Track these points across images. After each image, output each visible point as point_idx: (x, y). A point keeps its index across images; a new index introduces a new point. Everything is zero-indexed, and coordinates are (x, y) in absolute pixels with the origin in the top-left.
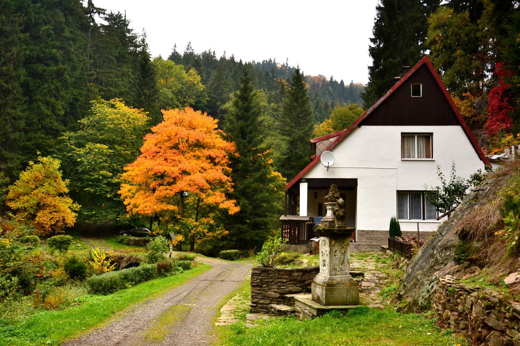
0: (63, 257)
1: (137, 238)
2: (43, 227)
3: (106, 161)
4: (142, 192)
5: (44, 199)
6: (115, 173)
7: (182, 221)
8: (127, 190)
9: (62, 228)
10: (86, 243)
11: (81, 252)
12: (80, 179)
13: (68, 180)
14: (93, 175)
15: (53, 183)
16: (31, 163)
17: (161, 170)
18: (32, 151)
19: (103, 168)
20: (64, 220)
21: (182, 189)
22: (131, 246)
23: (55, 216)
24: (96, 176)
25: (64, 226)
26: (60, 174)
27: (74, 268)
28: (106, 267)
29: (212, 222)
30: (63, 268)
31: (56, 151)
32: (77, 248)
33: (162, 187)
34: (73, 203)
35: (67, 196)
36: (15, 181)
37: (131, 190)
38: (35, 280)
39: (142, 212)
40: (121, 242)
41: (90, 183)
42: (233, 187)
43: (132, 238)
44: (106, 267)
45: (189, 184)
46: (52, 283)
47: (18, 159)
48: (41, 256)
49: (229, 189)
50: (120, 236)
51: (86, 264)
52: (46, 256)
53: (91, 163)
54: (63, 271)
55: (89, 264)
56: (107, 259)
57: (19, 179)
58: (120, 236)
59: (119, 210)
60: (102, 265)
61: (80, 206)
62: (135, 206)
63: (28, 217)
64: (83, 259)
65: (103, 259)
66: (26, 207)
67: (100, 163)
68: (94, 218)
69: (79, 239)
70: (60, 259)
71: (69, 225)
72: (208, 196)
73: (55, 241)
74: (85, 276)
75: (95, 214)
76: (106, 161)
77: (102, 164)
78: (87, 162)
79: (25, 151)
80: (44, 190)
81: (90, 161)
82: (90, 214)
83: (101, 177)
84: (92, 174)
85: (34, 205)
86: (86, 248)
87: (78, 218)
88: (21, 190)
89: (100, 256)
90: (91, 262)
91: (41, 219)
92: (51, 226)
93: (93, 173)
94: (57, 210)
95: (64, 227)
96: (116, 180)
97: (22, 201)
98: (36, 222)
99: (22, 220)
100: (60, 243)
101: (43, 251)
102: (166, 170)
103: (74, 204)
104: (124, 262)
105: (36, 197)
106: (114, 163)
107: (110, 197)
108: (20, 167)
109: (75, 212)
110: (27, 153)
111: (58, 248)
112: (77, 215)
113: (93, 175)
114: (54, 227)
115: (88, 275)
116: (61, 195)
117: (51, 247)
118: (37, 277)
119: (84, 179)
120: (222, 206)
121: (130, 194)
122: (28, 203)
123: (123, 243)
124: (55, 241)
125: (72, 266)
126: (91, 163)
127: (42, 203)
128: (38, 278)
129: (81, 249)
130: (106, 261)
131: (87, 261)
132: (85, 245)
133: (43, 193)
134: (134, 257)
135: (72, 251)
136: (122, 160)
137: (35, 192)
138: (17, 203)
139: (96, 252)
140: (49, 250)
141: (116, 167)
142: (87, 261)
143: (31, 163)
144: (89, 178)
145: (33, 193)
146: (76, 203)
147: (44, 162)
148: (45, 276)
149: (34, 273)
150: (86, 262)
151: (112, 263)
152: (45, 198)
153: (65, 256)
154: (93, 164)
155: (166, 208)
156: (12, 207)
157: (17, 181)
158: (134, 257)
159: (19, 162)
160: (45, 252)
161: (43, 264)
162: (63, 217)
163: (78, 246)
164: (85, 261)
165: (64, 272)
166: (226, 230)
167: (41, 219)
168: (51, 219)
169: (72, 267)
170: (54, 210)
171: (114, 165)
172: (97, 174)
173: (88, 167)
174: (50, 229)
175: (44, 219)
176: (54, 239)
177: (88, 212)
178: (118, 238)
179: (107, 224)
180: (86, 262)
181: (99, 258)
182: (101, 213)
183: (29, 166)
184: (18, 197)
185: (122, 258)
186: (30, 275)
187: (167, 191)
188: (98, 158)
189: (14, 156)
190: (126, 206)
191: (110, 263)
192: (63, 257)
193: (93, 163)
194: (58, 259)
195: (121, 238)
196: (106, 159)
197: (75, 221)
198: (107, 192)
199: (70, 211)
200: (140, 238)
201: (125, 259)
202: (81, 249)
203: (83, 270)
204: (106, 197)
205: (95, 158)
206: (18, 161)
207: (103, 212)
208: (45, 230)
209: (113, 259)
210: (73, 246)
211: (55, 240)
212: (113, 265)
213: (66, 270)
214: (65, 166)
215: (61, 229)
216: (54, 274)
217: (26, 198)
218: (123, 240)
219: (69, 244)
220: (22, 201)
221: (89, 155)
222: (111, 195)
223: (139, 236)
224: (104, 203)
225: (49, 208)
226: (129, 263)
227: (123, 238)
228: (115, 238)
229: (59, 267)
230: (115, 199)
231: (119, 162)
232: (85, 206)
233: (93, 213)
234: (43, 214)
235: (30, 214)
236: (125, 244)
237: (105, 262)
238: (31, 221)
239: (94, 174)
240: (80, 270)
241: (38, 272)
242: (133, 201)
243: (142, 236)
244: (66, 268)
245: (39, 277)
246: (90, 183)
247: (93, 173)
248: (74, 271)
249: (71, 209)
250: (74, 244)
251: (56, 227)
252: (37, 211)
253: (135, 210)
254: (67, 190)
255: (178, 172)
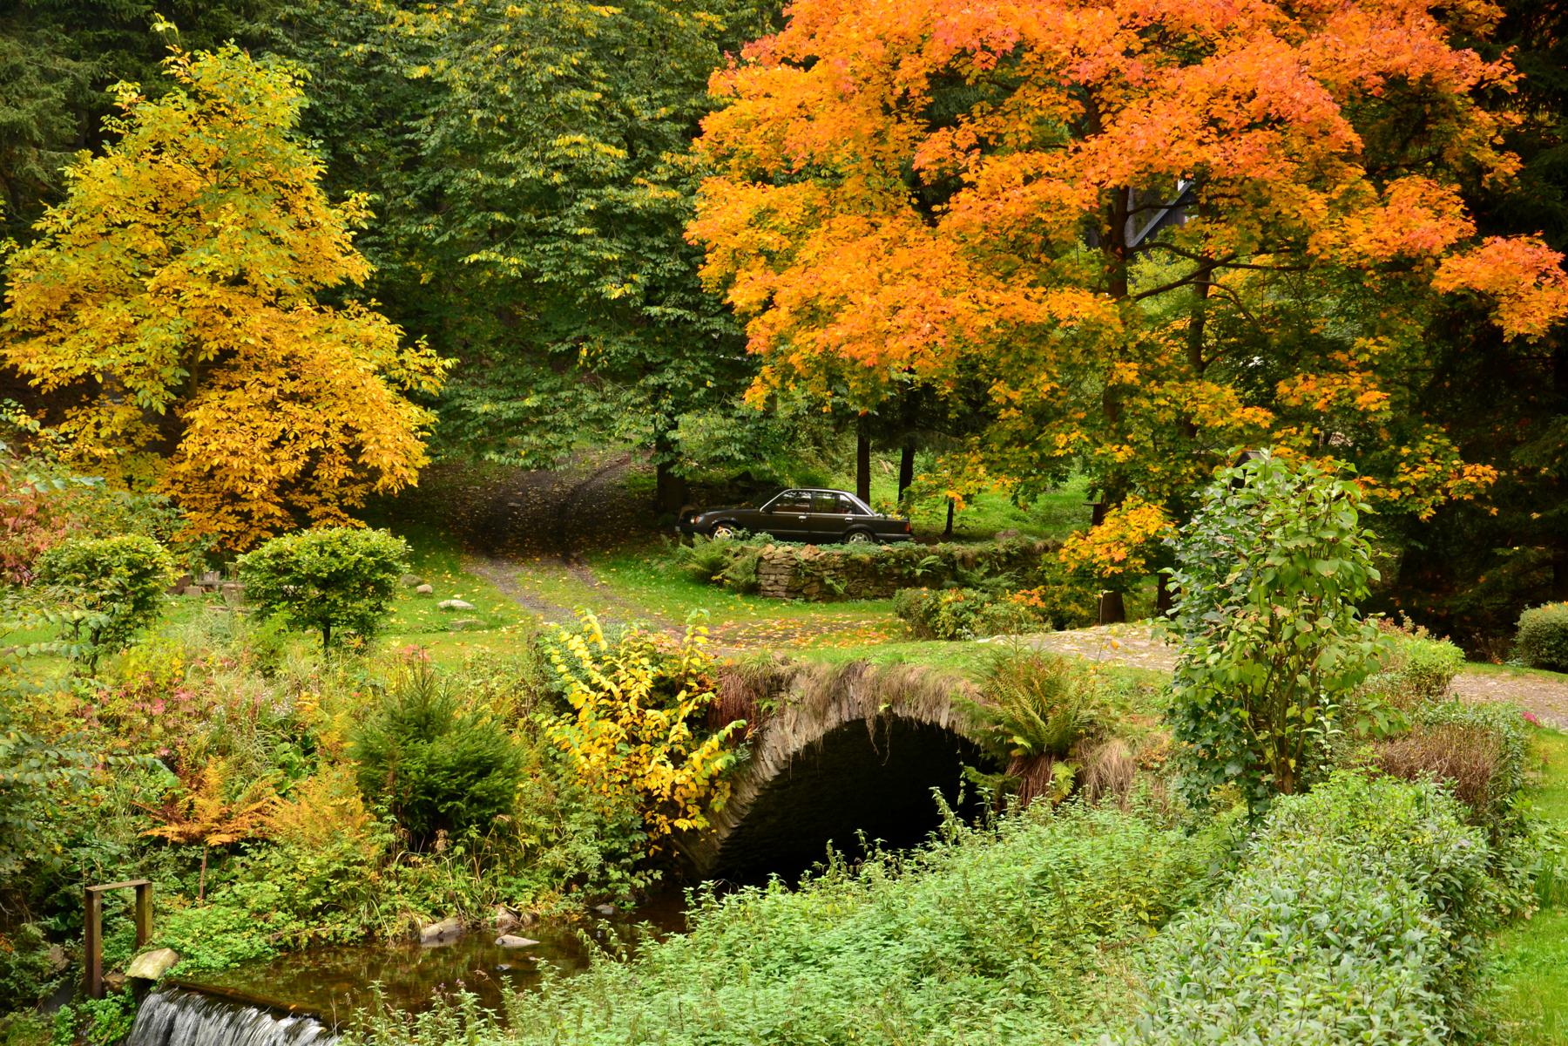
0: (346, 683)
1: (804, 552)
2: (234, 497)
3: (580, 77)
4: (845, 223)
5: (220, 318)
6: (643, 151)
7: (1146, 404)
8: (746, 212)
9: (348, 502)
10: (496, 590)
11: (474, 648)
12: (433, 202)
13: (364, 198)
14: (509, 169)
15: (269, 216)
16: (125, 93)
17: (997, 31)
18: (135, 35)
19: (571, 118)
20: (355, 451)
21: (1161, 163)
22: (774, 598)
23: (298, 427)
24: (532, 172)
25: (359, 490)
26: (308, 164)
27: (431, 769)
28: (660, 753)
29: (1373, 400)
30: (347, 772)
31: (279, 32)
32: (446, 623)
33: (997, 168)
34: (403, 345)
35: (362, 302)
36: (38, 213)
37: (771, 212)
38: (143, 871)
39: (867, 352)
40: (708, 577)
41: (499, 216)
42: (1512, 142)
43: (778, 550)
44: (660, 753)
45: (1214, 122)
46: (268, 891)
47: (48, 76)
48: (193, 682)
49: (1488, 155)
50: (697, 538)
51: (517, 738)
52: (221, 681)
53: (490, 89)
54: (347, 793)
55: (533, 730)
56: (664, 692)
57: (64, 199)
58: (697, 538)
59: (679, 382)
60: (634, 740)
61: (448, 363)
62: (811, 315)
63: (139, 441)
64: (489, 695)
65: (634, 696)
66: (119, 371)
67: (548, 88)
68: (532, 438)
69: (454, 570)
70: (325, 706)
71: (384, 479)
72: (1347, 210)
73: (288, 571)
74: (512, 827)
75: (538, 411)
76: (580, 77)
77: (559, 98)
78: (473, 87)
79: (90, 35)
80: (214, 263)
81: (486, 79)
82: (508, 411)
83: (558, 178)
84: (506, 158)
85: (163, 361)
86: (503, 622)
87: (437, 440)
88: (78, 268)
89: (613, 669)
90: (543, 718)
91: (213, 446)
92: (283, 487)
93: (512, 152)
94: (311, 388)
95: (363, 498)
96: (654, 192)
97: (92, 334)
98: (184, 468)
99: (100, 452)
100: (325, 584)
101: (202, 642)
102: (1034, 31)
103: (408, 354)
104: (790, 715)
105: (172, 311)
106: (632, 91)
107: (624, 300)
108: (68, 125)
109: (426, 401)
110: (105, 45)
111: (311, 621)
112: (431, 416)
113: (509, 169)
114: (300, 499)
115: (531, 820)
116: (330, 298)
117: (261, 616)
118: (161, 842)
119: (457, 194)
120: (1454, 275)
121: (770, 239)
122: (126, 347)
123: (720, 584)
124: (288, 571)
125: (413, 755)
126: (490, 89)
127: (214, 346)
128: (165, 853)
129: (470, 627)
130: (659, 706)
131: (519, 713)
132: (494, 600)
133: (213, 277)
134: (869, 673)
135: (412, 642)
136: (679, 73)
137: (163, 275)
138: (61, 349)
139: (578, 647)
140: (248, 633)
141: (647, 115)
142: (519, 713)
143: (125, 93)
144: (488, 187)
145: (151, 283)
146: (422, 342)
147: (206, 84)
148: (214, 840)
149: (137, 812)
150: (511, 723)
151: (701, 724)
152: (228, 314)
153: (359, 676)
154: (504, 100)
155: (1036, 314)
156: (31, 376)
157: (50, 211)
158: (869, 673)
159: (58, 94)
160: (217, 655)
161: (203, 739)
162: (347, 429)
163: (451, 609)
164: (507, 710)
165: (356, 802)
166: (1469, 456)
167: (213, 446)
168: (276, 444)
169: (415, 766)
170: (289, 387)
171: (632, 101)
172: (533, 161)
173: (478, 114)
174: (272, 509)
175: (232, 445)
176: (279, 555)
177: (495, 399)
178: (690, 555)
179: (600, 481)
180: (511, 723)
181: (607, 684)
182: (576, 400)
183: (117, 112)
184: (66, 313)
185: (776, 685)
186: (110, 830)
187: (1040, 185)
188: (536, 59)
189: (20, 59)
190: (746, 317)
191: (690, 721)
192: (346, 683)
193: (505, 90)
194: (310, 701)
195: (702, 551)
196: (582, 69)
197: (426, 461)
198: (602, 269)
199: (389, 393)
200: (824, 550)
201: (801, 688)
202: (470, 627)
203: (497, 780)
204: (599, 302)
205: (517, 62)
206: (46, 88)
207: (588, 395)
208: (246, 517)
209: (707, 696)
210: (423, 611)
211: (282, 567)
212: (714, 741)
213: (370, 789)
214: (340, 125)
215: (341, 507)
216: (285, 816)
217: (115, 313)
218: (715, 566)
219: (383, 590)
220: (92, 334)
221: (478, 44)
222: (628, 288)
223: (814, 540)
224: (586, 339)
225: (262, 376)
226: (832, 721)
227: (716, 555)
228: (669, 555)
229: (322, 766)
230: (655, 310)
231: (664, 83)
232: (470, 368)
233: (528, 402)
234: (222, 415)
235: (149, 415)
236: (734, 590)
237: (656, 716)
238: (160, 463)
239: (518, 157)
240: (477, 788)
241: (169, 807)
242: (792, 287)
243: (830, 540)
244: (372, 771)
245: (176, 846)
246: (499, 216)
247: (512, 152)
248: (431, 790)
249: (390, 381)
250: (424, 594)
251: (313, 498)
252: (185, 393)
253: (807, 345)
254: (360, 268)
255: (1119, 44)
